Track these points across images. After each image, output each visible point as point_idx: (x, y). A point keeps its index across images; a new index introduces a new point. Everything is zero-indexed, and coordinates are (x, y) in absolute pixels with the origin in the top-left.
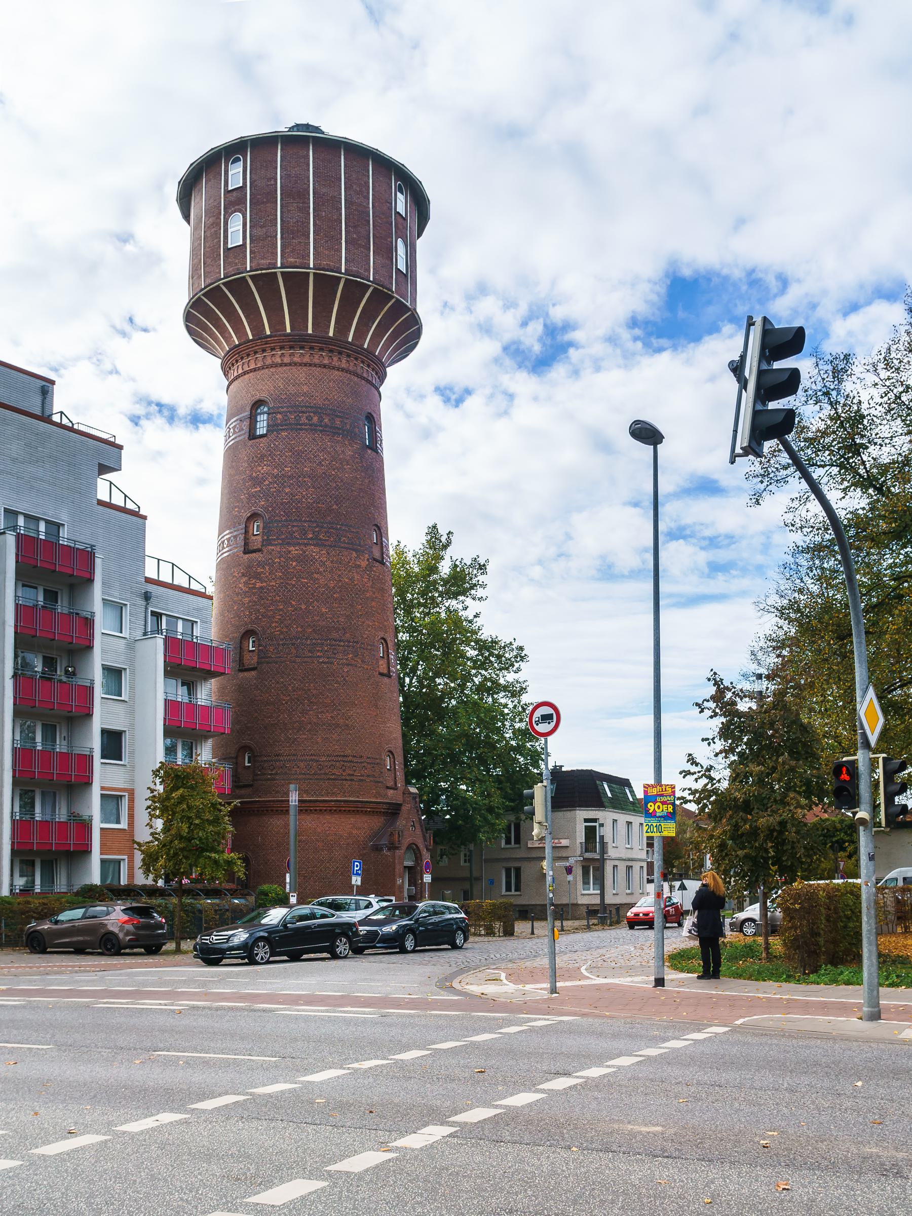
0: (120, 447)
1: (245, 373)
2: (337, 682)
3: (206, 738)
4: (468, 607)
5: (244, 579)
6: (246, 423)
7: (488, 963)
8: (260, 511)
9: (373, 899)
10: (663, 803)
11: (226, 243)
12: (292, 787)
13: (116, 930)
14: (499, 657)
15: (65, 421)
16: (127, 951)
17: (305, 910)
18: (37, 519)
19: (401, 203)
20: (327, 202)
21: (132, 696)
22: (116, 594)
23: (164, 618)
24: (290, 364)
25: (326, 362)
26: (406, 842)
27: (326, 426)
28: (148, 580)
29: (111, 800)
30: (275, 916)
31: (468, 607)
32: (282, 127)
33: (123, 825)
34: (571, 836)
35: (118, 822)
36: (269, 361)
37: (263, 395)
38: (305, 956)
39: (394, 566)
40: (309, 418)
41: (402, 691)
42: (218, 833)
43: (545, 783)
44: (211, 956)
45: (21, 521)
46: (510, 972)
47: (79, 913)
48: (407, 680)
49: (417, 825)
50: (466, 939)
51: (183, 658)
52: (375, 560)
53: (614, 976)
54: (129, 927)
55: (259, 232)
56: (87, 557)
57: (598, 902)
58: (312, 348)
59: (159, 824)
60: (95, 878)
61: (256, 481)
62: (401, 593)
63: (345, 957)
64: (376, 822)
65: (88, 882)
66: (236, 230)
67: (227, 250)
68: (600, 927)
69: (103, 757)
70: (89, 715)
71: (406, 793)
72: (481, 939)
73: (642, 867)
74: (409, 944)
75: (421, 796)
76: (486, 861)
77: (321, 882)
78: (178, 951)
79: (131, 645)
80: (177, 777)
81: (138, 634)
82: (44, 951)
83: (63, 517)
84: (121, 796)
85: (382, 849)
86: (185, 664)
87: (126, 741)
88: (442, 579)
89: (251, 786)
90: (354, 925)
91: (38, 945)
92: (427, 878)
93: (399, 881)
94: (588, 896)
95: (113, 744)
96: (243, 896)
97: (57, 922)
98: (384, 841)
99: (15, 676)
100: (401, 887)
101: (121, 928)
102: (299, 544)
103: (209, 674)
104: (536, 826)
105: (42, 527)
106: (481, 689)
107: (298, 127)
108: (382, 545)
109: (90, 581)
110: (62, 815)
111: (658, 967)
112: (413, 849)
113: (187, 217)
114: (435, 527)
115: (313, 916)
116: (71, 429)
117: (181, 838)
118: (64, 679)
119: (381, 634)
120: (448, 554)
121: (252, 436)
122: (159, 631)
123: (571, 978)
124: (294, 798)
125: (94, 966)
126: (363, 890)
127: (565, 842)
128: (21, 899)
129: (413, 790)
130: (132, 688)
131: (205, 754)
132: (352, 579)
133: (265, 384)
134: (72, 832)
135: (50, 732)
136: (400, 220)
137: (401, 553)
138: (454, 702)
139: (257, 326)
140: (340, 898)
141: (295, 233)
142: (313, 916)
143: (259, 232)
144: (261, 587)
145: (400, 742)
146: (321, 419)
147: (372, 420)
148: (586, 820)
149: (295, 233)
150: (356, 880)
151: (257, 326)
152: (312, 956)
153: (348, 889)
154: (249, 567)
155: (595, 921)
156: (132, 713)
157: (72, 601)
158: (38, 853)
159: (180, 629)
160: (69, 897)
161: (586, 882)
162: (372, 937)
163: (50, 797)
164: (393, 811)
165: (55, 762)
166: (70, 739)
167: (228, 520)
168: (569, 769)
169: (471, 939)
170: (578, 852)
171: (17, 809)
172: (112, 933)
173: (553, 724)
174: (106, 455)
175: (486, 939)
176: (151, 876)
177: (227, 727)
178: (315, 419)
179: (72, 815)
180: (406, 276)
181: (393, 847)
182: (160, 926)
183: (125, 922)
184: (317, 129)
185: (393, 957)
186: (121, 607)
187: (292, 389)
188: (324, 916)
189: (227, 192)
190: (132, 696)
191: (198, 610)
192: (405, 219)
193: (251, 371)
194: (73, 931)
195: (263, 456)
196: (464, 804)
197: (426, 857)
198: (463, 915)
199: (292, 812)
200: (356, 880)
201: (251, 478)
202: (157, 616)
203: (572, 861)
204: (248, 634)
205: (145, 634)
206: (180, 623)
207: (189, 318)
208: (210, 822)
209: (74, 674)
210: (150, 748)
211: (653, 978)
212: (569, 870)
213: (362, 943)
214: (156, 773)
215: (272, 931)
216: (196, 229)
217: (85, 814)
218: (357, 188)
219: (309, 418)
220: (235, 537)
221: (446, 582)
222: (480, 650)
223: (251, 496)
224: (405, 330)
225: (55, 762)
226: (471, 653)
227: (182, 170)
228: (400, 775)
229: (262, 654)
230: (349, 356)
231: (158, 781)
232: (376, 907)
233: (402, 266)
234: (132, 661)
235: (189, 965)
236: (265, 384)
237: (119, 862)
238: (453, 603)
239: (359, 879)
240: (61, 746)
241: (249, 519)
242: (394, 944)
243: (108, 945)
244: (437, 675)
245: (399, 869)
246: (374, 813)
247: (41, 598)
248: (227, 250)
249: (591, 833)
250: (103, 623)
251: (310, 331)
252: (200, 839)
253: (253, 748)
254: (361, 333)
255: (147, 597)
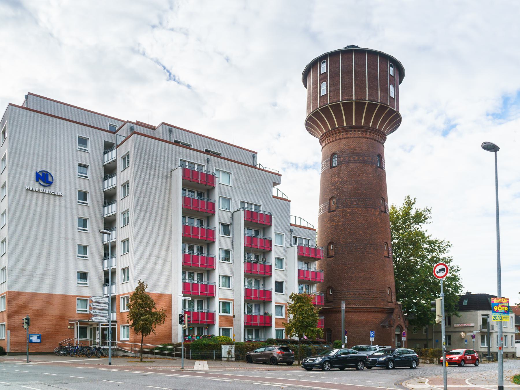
0: (281, 175)
1: (328, 143)
2: (366, 260)
3: (314, 284)
4: (423, 227)
5: (329, 222)
6: (329, 162)
7: (425, 375)
8: (335, 195)
9: (377, 347)
10: (502, 306)
11: (320, 94)
12: (342, 302)
13: (276, 356)
14: (438, 247)
15: (261, 167)
16: (281, 363)
17: (346, 350)
18: (252, 204)
19: (392, 71)
20: (360, 74)
21: (286, 269)
22: (280, 230)
23: (298, 239)
24: (346, 138)
25: (361, 135)
26: (396, 324)
27: (361, 160)
28: (292, 225)
29: (279, 307)
30: (334, 352)
31: (423, 227)
32: (342, 46)
33: (284, 317)
34: (476, 322)
35: (282, 316)
36: (338, 138)
37: (336, 151)
38: (346, 369)
39: (391, 213)
40: (354, 158)
41: (396, 263)
42: (314, 320)
43: (441, 298)
44: (309, 368)
45: (246, 205)
46: (431, 379)
47: (263, 349)
48: (398, 259)
49: (402, 318)
50: (417, 365)
51: (305, 254)
52: (382, 211)
53: (480, 384)
54: (280, 355)
55: (333, 88)
56: (269, 217)
57: (487, 351)
58: (355, 131)
59: (292, 316)
60: (273, 336)
61: (333, 184)
62: (395, 224)
63: (362, 370)
64: (383, 316)
65: (270, 338)
66: (324, 89)
67: (321, 97)
68: (487, 362)
69: (276, 291)
70: (270, 276)
71: (396, 304)
72: (427, 365)
73: (512, 336)
74: (391, 365)
75: (403, 306)
76: (435, 332)
77: (359, 339)
78: (299, 364)
79: (286, 249)
80: (298, 298)
81: (288, 245)
82: (252, 363)
83: (261, 203)
84: (87, 300)
85: (386, 327)
86: (306, 256)
87: (284, 285)
88: (412, 217)
89: (332, 302)
90: (366, 357)
91: (250, 360)
92: (404, 339)
93: (393, 340)
94: (483, 348)
95: (280, 286)
96: (328, 344)
97: (256, 352)
98: (387, 324)
99: (245, 262)
100: (394, 342)
101: (278, 355)
102: (350, 207)
103: (315, 259)
104: (437, 317)
105: (253, 207)
106: (432, 261)
107: (349, 47)
108: (385, 206)
109: (270, 226)
110: (262, 313)
111: (500, 381)
112: (400, 327)
113: (306, 86)
114: (408, 197)
115: (349, 353)
116: (263, 170)
117: (300, 322)
118: (262, 263)
119: (385, 241)
120: (414, 207)
121: (331, 167)
122: (296, 244)
123: (454, 383)
124: (343, 306)
125: (266, 369)
126: (374, 344)
127: (472, 325)
128: (247, 343)
129: (399, 303)
130: (286, 266)
131: (314, 290)
132: (372, 220)
133: (336, 147)
134: (265, 319)
135: (257, 282)
136: (391, 77)
137: (393, 208)
138: (419, 267)
139: (332, 125)
140: (365, 346)
141: (347, 87)
142: (349, 353)
143: (333, 88)
144: (335, 225)
145: (394, 284)
146: (359, 158)
147: (380, 157)
148: (483, 315)
149: (347, 87)
150: (372, 339)
151: (332, 125)
152: (350, 369)
153: (369, 343)
154: (331, 217)
155: (485, 359)
156: (286, 275)
157: (264, 234)
158: (253, 327)
159: (304, 243)
160: (263, 343)
161: (483, 342)
162: (374, 362)
163: (258, 306)
164: (391, 311)
165: (259, 293)
166: (264, 285)
167: (323, 200)
168: (474, 293)
169: (420, 365)
170: (479, 329)
171: (246, 310)
172: (274, 357)
173: (445, 273)
174: (275, 179)
175: (429, 365)
176: (289, 336)
177: (322, 279)
178: (356, 158)
179: (266, 313)
180: (394, 99)
181: (390, 326)
182: (292, 355)
183: (279, 353)
184: (357, 47)
185: (383, 371)
186: (282, 236)
187: (347, 148)
188: (353, 353)
189: (320, 75)
190: (286, 269)
191: (311, 235)
192: (394, 77)
193: (331, 142)
194: (261, 356)
195: (336, 175)
196: (423, 309)
197: (405, 330)
198: (416, 355)
199: (343, 312)
200: (372, 339)
201: (331, 183)
202: (295, 238)
203: (474, 333)
204: (330, 243)
205: (291, 245)
206: (304, 240)
207: (307, 124)
208: (310, 316)
209: (265, 261)
210: (293, 287)
211: (497, 386)
212: (473, 337)
213: (371, 365)
214: (290, 297)
215: (332, 358)
216: (309, 90)
217: (269, 313)
218: (373, 67)
219: (354, 158)
220: (325, 206)
221: (413, 218)
222: (430, 245)
223: (331, 190)
224: (394, 119)
225: (259, 293)
226: (426, 246)
227: (303, 68)
228: (394, 297)
229: (336, 251)
230: (370, 132)
231: (291, 300)
232: (378, 350)
233: (392, 95)
234: (286, 255)
235: (300, 370)
236: (336, 147)
237: (282, 330)
238: (416, 226)
239: (373, 339)
240: (261, 288)
241: (330, 199)
242: (384, 365)
243: (271, 361)
244: (410, 256)
245: (393, 335)
246: (382, 312)
247: (253, 233)
248: (321, 97)
249: (485, 322)
250: (275, 241)
251: (354, 124)
252: (307, 322)
253: (333, 287)
254: (375, 123)
255: (291, 231)
